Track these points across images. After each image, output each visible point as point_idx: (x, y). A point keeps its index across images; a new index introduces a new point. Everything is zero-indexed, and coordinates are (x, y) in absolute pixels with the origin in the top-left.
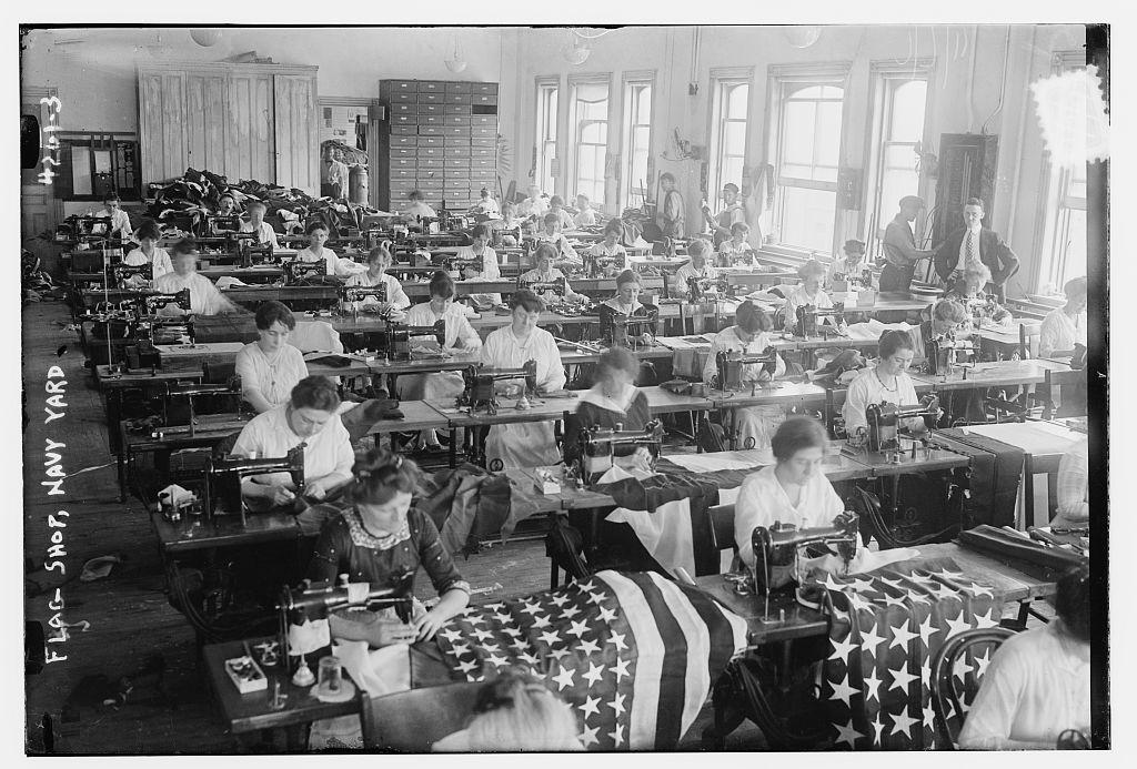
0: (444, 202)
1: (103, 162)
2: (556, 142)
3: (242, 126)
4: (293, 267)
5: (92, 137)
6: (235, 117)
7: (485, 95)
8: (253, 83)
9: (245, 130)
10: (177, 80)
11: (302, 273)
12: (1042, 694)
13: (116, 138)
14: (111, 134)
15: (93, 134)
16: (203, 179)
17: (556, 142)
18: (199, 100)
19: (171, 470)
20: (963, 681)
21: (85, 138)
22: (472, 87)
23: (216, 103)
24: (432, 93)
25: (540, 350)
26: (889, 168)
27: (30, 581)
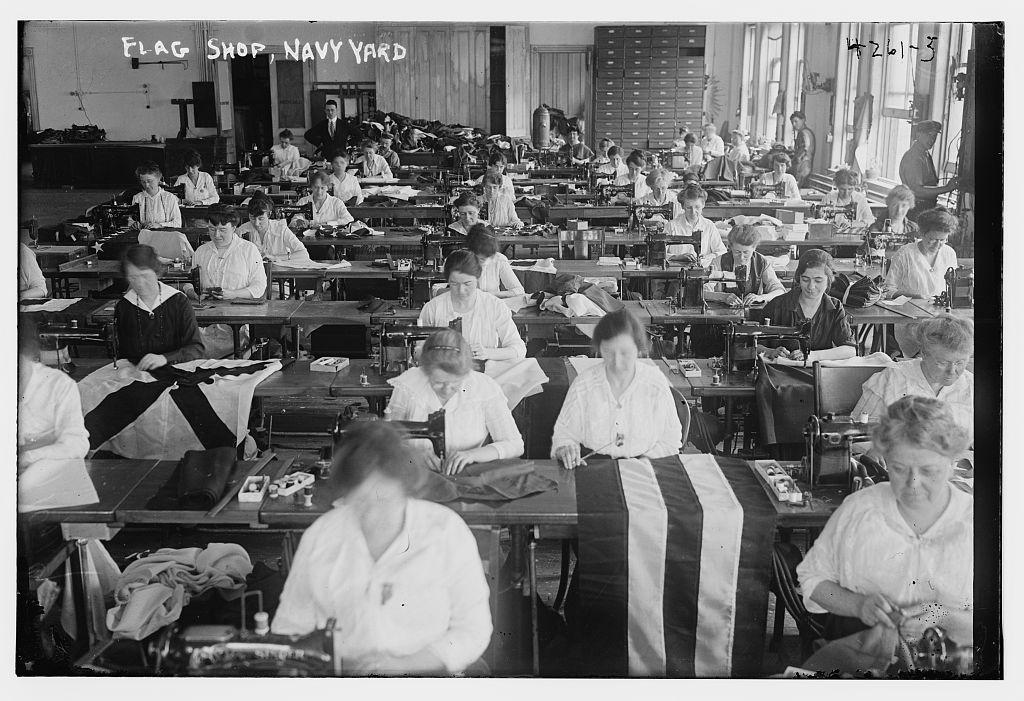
0: (648, 142)
1: (351, 109)
2: (780, 82)
3: (462, 74)
4: (637, 211)
5: (356, 87)
6: (456, 66)
7: (692, 37)
8: (472, 36)
9: (465, 78)
10: (407, 35)
11: (647, 217)
12: (191, 569)
13: (361, 87)
14: (356, 84)
15: (341, 84)
16: (388, 119)
17: (780, 82)
18: (426, 52)
19: (742, 434)
20: (787, 613)
21: (337, 87)
22: (678, 31)
23: (439, 54)
24: (639, 38)
25: (236, 259)
26: (891, 94)
27: (695, 556)
